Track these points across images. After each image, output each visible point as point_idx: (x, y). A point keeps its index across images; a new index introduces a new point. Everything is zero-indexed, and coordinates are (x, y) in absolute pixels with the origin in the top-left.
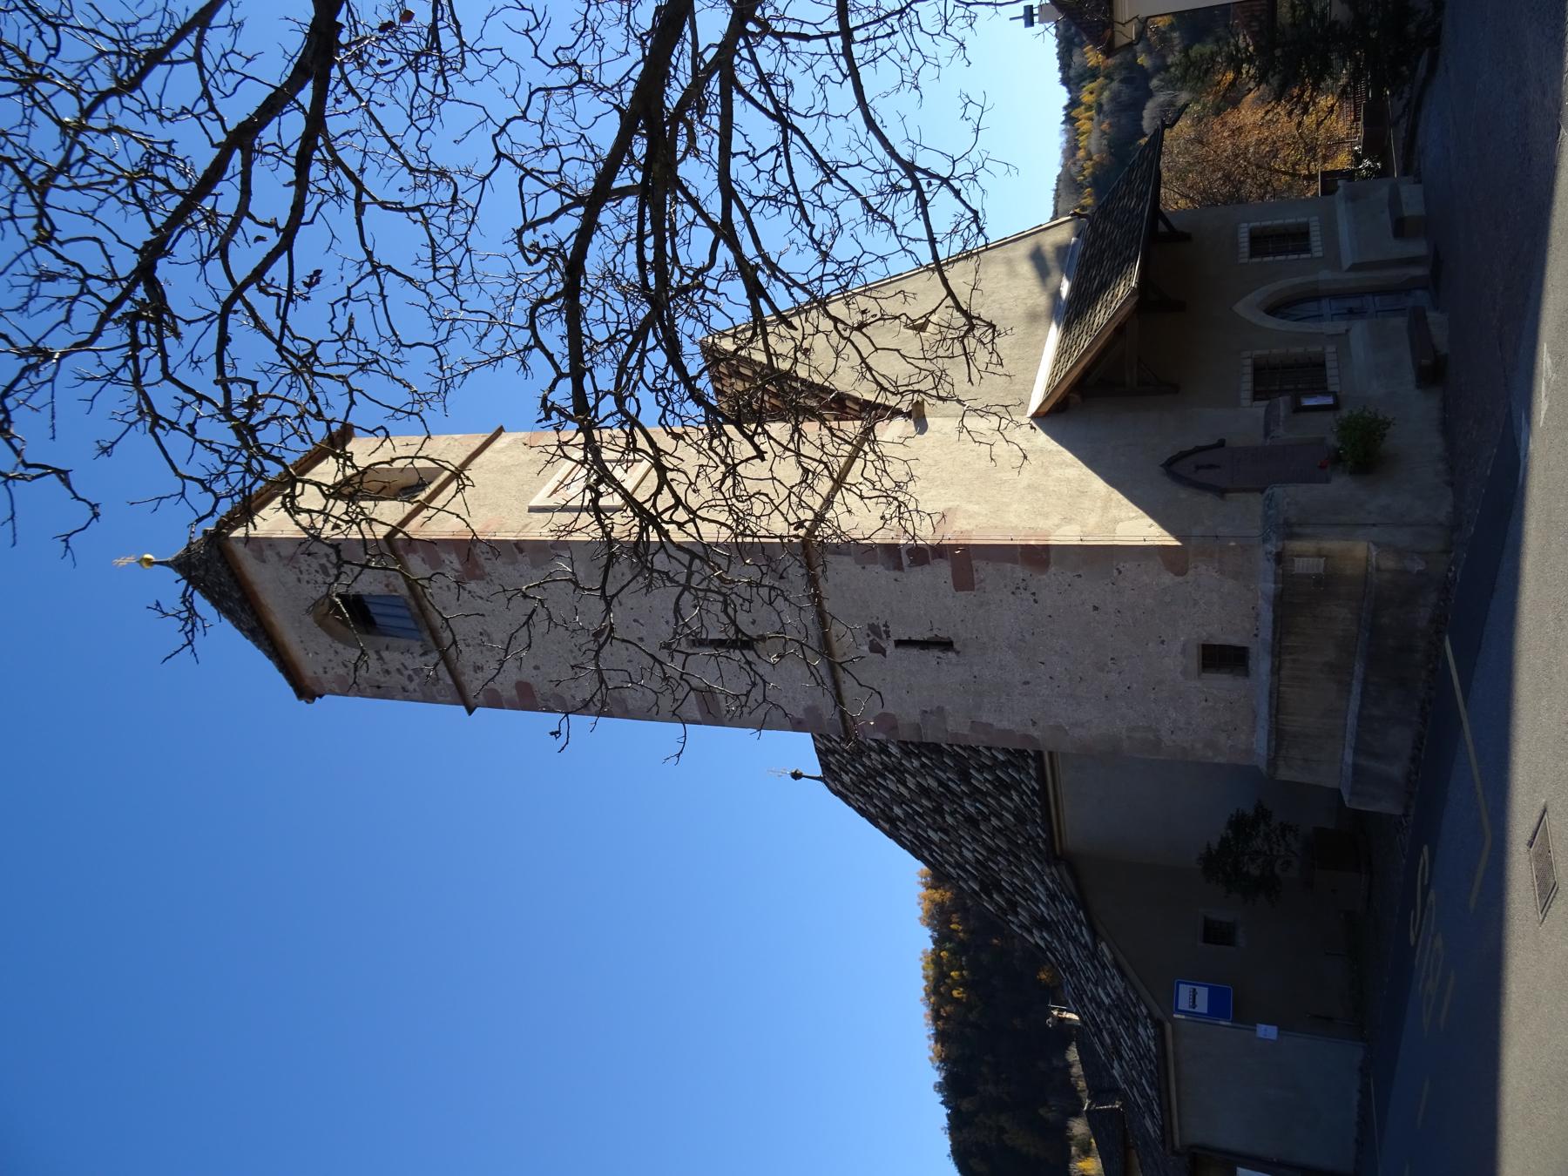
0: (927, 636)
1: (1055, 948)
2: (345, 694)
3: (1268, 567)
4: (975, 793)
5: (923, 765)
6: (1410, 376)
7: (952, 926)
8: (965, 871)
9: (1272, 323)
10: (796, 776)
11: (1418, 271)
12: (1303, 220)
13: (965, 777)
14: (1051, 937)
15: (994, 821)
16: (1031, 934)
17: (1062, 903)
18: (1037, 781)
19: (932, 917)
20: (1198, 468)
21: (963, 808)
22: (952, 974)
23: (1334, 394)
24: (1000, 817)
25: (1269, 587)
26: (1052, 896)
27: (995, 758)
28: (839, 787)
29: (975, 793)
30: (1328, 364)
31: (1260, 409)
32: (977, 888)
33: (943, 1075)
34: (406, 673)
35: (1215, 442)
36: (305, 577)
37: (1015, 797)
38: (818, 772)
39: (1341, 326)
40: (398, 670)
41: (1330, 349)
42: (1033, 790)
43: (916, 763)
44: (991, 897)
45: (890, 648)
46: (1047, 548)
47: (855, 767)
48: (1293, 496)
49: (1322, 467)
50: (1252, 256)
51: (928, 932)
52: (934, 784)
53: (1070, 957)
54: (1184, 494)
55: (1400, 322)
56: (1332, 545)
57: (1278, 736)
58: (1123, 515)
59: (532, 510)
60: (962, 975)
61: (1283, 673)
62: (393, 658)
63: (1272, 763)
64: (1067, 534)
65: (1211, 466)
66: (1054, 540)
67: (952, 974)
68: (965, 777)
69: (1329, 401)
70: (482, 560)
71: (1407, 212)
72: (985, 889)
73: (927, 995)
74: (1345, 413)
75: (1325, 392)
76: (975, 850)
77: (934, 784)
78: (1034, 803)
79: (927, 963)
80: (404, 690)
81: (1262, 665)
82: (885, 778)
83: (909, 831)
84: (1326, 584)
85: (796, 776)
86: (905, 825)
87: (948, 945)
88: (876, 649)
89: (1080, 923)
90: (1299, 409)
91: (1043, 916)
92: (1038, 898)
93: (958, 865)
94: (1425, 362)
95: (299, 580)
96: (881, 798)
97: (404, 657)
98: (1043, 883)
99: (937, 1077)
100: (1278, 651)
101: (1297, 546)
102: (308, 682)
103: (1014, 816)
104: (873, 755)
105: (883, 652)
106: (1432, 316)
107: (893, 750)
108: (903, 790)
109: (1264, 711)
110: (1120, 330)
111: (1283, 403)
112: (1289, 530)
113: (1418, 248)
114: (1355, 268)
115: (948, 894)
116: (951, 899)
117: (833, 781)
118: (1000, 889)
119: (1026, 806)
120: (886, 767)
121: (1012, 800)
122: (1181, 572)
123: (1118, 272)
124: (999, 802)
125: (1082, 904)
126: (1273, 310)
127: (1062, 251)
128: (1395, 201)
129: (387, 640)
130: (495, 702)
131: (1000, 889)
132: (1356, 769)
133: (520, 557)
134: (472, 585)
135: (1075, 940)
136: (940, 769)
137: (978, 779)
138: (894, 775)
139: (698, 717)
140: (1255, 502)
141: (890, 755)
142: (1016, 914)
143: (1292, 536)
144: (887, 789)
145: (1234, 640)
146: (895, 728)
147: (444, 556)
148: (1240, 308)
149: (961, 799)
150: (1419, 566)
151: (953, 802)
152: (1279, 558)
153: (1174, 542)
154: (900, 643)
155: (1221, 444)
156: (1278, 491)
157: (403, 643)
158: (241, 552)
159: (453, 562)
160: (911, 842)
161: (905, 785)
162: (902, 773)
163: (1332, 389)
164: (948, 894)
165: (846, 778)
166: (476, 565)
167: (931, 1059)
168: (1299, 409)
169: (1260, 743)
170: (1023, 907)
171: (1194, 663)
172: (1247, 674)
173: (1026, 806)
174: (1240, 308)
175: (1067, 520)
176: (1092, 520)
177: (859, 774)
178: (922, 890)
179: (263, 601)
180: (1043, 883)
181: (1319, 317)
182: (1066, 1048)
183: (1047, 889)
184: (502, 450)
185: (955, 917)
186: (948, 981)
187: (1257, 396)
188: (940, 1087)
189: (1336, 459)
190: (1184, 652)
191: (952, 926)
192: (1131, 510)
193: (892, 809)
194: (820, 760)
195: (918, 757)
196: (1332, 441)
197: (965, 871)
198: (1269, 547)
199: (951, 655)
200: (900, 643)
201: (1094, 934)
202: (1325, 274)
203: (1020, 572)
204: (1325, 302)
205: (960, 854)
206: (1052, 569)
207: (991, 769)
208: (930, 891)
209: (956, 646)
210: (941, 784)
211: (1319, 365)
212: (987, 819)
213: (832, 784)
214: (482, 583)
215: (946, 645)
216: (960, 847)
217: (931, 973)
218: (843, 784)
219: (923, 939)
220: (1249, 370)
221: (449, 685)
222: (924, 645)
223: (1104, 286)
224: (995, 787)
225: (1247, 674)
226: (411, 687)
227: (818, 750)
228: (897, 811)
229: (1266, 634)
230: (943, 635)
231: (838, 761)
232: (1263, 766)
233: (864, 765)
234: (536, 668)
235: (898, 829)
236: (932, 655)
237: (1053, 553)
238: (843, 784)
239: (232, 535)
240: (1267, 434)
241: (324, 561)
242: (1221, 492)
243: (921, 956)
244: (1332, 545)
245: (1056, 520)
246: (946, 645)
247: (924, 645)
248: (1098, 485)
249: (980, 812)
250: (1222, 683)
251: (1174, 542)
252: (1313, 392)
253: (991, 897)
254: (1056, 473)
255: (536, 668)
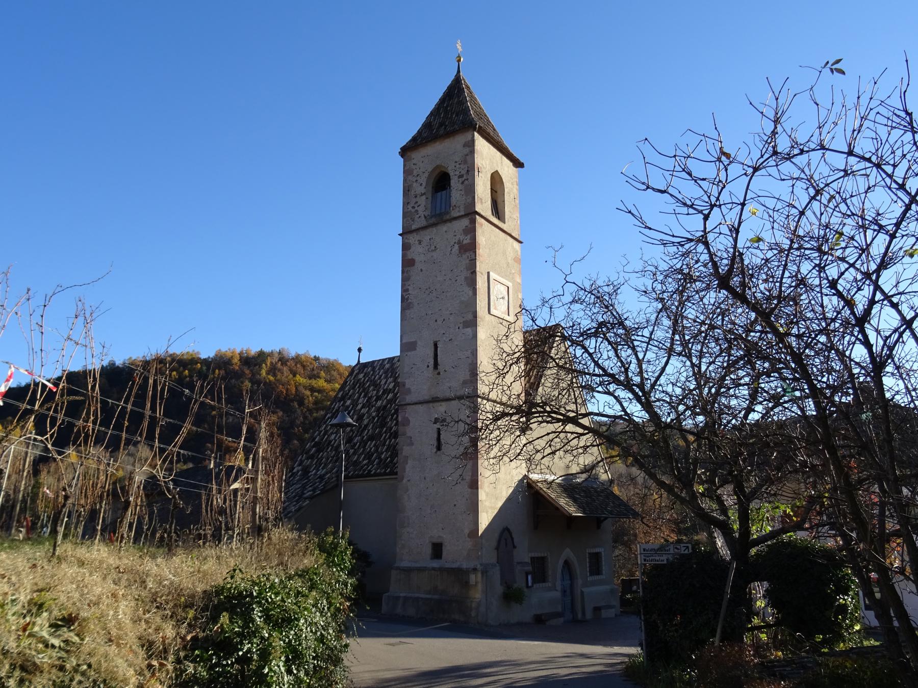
0: (442, 441)
1: (295, 477)
2: (404, 172)
3: (471, 565)
4: (364, 443)
5: (374, 418)
6: (539, 612)
7: (217, 371)
8: (324, 435)
9: (561, 562)
10: (360, 350)
11: (580, 616)
12: (604, 572)
13: (371, 438)
14: (300, 475)
15: (352, 451)
16: (299, 465)
17: (320, 482)
18: (375, 473)
19: (221, 357)
20: (506, 540)
21: (356, 436)
22: (187, 371)
23: (532, 586)
24: (354, 453)
25: (464, 566)
26: (321, 477)
27: (382, 453)
28: (356, 372)
29: (364, 443)
30: (544, 584)
31: (528, 560)
32: (316, 440)
33: (120, 366)
34: (416, 206)
35: (515, 544)
36: (458, 166)
37: (365, 462)
38: (362, 361)
39: (559, 587)
40: (417, 202)
41: (550, 585)
42: (370, 471)
43: (374, 414)
44: (313, 446)
45: (438, 426)
46: (477, 488)
47: (367, 381)
48: (496, 573)
49: (506, 583)
50: (589, 553)
51: (212, 355)
52: (366, 422)
53: (293, 484)
54: (497, 535)
55: (559, 609)
56: (480, 586)
57: (408, 571)
58: (489, 514)
59: (488, 273)
60: (186, 377)
61: (433, 572)
62: (422, 200)
63: (398, 568)
64: (482, 495)
65: (506, 544)
66: (480, 490)
67: (187, 371)
68: (371, 438)
69: (530, 584)
70: (468, 254)
71: (603, 611)
72: (316, 445)
73: (171, 355)
74: (525, 590)
75: (533, 582)
76: (336, 441)
77: (366, 422)
78: (364, 471)
79: (191, 355)
80: (408, 203)
81: (436, 564)
82: (365, 397)
83: (339, 407)
84: (466, 585)
85: (360, 350)
86: (342, 405)
87: (204, 368)
88: (436, 421)
89: (314, 490)
90: (527, 574)
91: (309, 472)
92: (318, 470)
93: (326, 432)
94: (543, 617)
95: (456, 162)
96: (354, 394)
97: (423, 205)
98: (327, 473)
99: (119, 362)
100: (441, 570)
101: (479, 575)
102: (409, 154)
103: (356, 461)
104: (375, 392)
105: (435, 423)
106: (562, 620)
107: (379, 403)
108: (359, 406)
109: (418, 565)
110: (557, 509)
111: (530, 568)
112: (485, 572)
113: (589, 615)
114: (582, 592)
115: (237, 368)
116: (233, 369)
117: (359, 369)
118: (318, 451)
119: (362, 467)
120: (370, 398)
121: (364, 460)
122: (469, 536)
123: (581, 506)
124: (361, 454)
125: (323, 492)
126: (567, 563)
127: (596, 478)
128: (609, 607)
129: (430, 198)
130: (406, 247)
131: (318, 451)
132: (398, 598)
133: (469, 272)
134: (457, 246)
135: (304, 487)
136: (373, 426)
137: (371, 445)
138: (367, 401)
139: (404, 341)
140: (494, 560)
141: (376, 401)
142: (307, 459)
143: (482, 573)
144: (359, 398)
145: (444, 554)
146: (404, 425)
147: (469, 237)
148: (568, 550)
149: (360, 435)
150: (473, 614)
151: (358, 432)
152: (475, 570)
153: (480, 533)
154: (439, 430)
155: (514, 547)
156: (498, 568)
157: (429, 206)
158: (468, 136)
159: (467, 240)
160: (334, 408)
161: (362, 408)
162: (368, 407)
163: (535, 586)
164: (237, 368)
165: (361, 376)
166: (466, 251)
167: (131, 358)
168: (527, 574)
169: (405, 564)
170: (311, 462)
171: (435, 541)
172: (431, 559)
173: (362, 467)
174: (568, 550)
175: (487, 494)
176: (487, 504)
177: (364, 384)
178: (238, 351)
179: (446, 140)
180: (327, 473)
181: (563, 580)
182: (193, 463)
183: (324, 475)
184: (512, 246)
185: (222, 372)
186: (181, 369)
187: (532, 558)
188: (112, 365)
189: (509, 587)
190: (440, 537)
191: (217, 371)
192: (491, 518)
193: (349, 399)
194: (369, 362)
195: (377, 416)
196: (515, 586)
197: (324, 435)
198: (479, 566)
199: (435, 450)
200: (439, 430)
201: (311, 498)
202: (580, 582)
203: (468, 478)
204: (569, 582)
205: (332, 433)
206: (470, 490)
207: (376, 451)
208: (238, 356)
209: (438, 452)
210: (366, 426)
211: (544, 580)
212: (352, 447)
213: (357, 368)
214: (458, 252)
215: (439, 448)
216: (336, 433)
217: (185, 357)
218: (358, 374)
219: (207, 353)
220: (543, 555)
221: (411, 226)
222: (439, 439)
223: (575, 500)
224: (368, 453)
225: (431, 559)
226: (410, 207)
227: (373, 362)
228: (349, 402)
229: (447, 565)
230: (443, 447)
231: (369, 373)
232: (396, 565)
233: (369, 386)
234: (421, 270)
235: (340, 401)
236: (436, 444)
237: (475, 490)
238: (358, 374)
239: (476, 134)
240: (518, 563)
241: (465, 177)
242: (497, 548)
243: (196, 351)
244: (480, 586)
245: (487, 490)
246: (439, 448)
247: (439, 439)
248: (500, 504)
249: (355, 445)
250: (428, 550)
251: (480, 533)
252: (533, 579)
253: (313, 446)
254: (504, 488)
255: (421, 270)
